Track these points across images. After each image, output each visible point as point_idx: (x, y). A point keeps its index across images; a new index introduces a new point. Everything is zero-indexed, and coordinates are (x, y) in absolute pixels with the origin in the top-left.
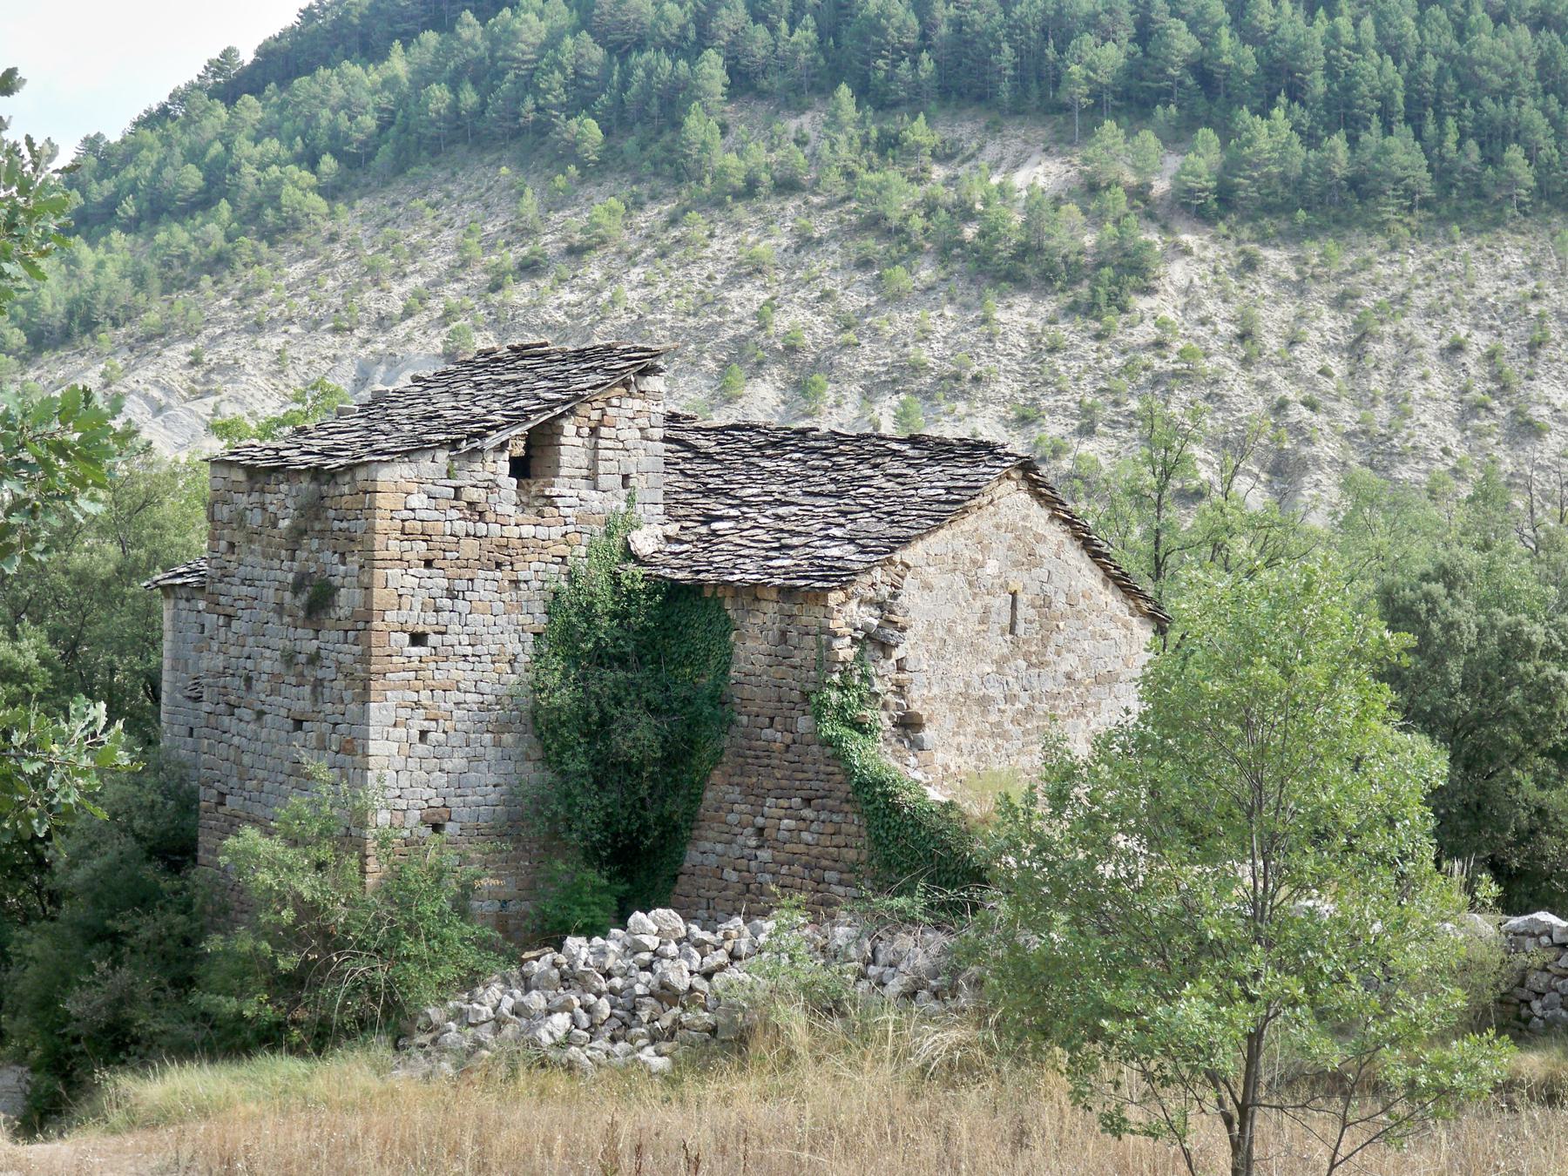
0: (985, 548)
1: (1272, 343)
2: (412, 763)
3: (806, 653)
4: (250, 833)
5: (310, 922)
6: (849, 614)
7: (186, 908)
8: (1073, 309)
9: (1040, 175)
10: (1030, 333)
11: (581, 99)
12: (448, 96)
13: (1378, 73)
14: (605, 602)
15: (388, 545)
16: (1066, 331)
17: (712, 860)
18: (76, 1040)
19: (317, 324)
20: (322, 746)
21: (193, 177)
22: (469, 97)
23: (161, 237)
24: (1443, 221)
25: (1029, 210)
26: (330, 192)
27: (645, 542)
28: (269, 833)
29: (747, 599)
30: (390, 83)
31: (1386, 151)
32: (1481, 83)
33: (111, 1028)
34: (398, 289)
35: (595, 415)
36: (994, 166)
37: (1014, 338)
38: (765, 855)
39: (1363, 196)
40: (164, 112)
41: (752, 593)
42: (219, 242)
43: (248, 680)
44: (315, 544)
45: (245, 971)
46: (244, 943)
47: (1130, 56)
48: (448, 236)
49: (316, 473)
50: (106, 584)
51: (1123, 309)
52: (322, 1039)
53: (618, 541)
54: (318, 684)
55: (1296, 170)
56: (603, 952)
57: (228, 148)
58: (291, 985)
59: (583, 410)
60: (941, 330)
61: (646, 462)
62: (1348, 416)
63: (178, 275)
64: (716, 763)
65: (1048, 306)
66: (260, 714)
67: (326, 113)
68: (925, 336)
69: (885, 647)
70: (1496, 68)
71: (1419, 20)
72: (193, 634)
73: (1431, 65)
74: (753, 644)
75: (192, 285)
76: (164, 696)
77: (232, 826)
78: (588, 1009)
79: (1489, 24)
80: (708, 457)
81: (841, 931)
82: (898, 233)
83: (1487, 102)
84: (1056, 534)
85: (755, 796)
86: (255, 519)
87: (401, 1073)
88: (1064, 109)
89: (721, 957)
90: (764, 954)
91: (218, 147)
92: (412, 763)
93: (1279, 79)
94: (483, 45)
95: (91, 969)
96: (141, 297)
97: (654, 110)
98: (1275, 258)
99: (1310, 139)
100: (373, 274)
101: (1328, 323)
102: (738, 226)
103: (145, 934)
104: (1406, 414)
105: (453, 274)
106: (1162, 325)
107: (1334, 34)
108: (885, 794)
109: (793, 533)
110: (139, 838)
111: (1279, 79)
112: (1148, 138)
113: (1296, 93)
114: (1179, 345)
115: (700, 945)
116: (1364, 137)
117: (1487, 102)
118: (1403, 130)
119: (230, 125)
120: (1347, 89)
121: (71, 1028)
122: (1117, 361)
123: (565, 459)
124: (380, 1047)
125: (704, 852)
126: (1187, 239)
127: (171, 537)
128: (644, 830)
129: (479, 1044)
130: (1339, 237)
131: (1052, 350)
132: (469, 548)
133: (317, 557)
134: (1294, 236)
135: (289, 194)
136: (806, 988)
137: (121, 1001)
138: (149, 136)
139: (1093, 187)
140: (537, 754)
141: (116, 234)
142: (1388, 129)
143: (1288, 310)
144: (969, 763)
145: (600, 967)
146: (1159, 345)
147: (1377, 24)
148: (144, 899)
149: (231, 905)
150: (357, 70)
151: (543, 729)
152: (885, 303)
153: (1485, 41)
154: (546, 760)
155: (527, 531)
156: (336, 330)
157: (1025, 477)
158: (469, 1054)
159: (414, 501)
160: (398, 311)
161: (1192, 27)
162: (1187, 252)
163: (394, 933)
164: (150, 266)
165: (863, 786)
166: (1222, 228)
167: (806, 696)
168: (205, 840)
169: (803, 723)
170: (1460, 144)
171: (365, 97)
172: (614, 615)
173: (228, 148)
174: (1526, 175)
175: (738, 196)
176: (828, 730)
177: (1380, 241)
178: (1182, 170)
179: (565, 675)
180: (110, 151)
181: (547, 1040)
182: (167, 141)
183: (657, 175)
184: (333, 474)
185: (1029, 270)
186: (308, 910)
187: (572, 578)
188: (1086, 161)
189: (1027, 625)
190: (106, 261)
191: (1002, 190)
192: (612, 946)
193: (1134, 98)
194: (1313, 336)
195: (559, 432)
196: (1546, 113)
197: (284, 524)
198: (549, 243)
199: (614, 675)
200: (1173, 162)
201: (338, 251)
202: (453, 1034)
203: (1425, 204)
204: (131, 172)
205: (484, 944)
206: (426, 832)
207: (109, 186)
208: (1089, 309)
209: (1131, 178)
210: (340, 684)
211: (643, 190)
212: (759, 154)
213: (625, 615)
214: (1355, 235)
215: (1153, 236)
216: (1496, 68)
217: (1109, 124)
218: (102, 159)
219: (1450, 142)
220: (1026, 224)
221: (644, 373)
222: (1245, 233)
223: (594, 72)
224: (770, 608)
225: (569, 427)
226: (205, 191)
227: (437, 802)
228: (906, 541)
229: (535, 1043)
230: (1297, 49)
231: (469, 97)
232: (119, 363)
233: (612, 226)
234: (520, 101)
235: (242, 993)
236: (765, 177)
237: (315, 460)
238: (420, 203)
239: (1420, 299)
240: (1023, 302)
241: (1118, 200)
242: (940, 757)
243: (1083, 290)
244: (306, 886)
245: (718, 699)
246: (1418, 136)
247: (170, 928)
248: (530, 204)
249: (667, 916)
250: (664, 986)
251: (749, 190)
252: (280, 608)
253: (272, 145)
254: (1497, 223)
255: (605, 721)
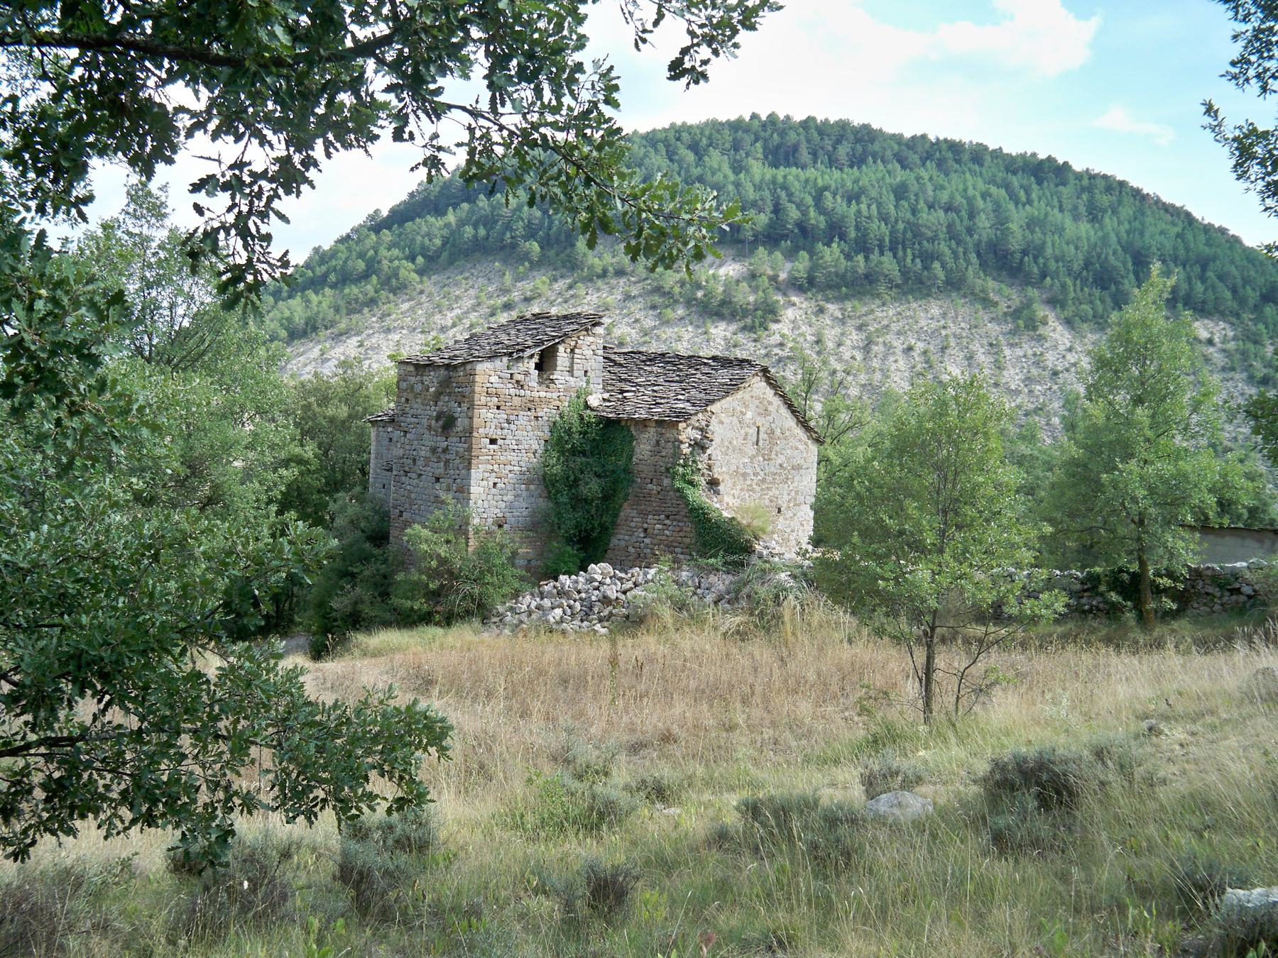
0: (747, 407)
1: (830, 345)
2: (490, 497)
3: (668, 450)
4: (417, 527)
5: (446, 570)
6: (688, 433)
7: (385, 561)
8: (744, 329)
9: (731, 270)
10: (725, 339)
11: (531, 234)
12: (473, 232)
13: (878, 229)
14: (576, 426)
15: (481, 399)
16: (741, 338)
17: (623, 543)
18: (335, 620)
19: (415, 329)
20: (448, 490)
21: (361, 265)
22: (482, 232)
23: (347, 291)
24: (905, 294)
25: (725, 285)
26: (421, 272)
27: (594, 401)
28: (425, 527)
29: (641, 427)
30: (447, 225)
31: (881, 263)
32: (922, 235)
33: (351, 615)
34: (450, 315)
35: (573, 343)
36: (711, 266)
37: (718, 340)
38: (647, 541)
39: (871, 282)
40: (348, 236)
41: (644, 423)
42: (371, 293)
43: (414, 460)
44: (447, 398)
45: (414, 589)
46: (415, 576)
47: (771, 219)
48: (472, 292)
49: (447, 366)
50: (343, 422)
51: (766, 329)
52: (448, 620)
53: (582, 400)
54: (447, 461)
55: (842, 270)
56: (576, 582)
57: (376, 252)
58: (435, 595)
59: (568, 340)
60: (686, 337)
61: (595, 366)
62: (863, 378)
63: (354, 308)
64: (626, 500)
65: (733, 327)
66: (420, 475)
67: (419, 238)
68: (679, 339)
69: (703, 448)
70: (929, 228)
71: (896, 207)
72: (386, 442)
73: (901, 226)
74: (643, 447)
75: (360, 312)
76: (573, 311)
77: (407, 524)
78: (570, 607)
79: (926, 209)
80: (621, 365)
81: (684, 573)
82: (669, 294)
83: (925, 243)
84: (777, 401)
85: (644, 514)
86: (418, 388)
87: (486, 635)
88: (742, 242)
89: (630, 584)
90: (651, 583)
91: (372, 252)
92: (490, 497)
93: (835, 230)
94: (488, 209)
95: (342, 588)
96: (338, 317)
97: (563, 238)
98: (832, 308)
99: (848, 257)
100: (439, 308)
101: (855, 337)
102: (598, 290)
103: (366, 573)
104: (888, 377)
105: (474, 309)
106: (783, 336)
107: (859, 212)
108: (704, 514)
109: (662, 398)
110: (363, 531)
111: (835, 230)
112: (778, 255)
113: (842, 237)
114: (790, 345)
115: (621, 579)
116: (872, 257)
117: (925, 243)
118: (889, 254)
119: (377, 242)
120: (864, 236)
121: (334, 614)
122: (763, 352)
123: (559, 362)
124: (476, 623)
125: (619, 539)
126: (794, 299)
127: (373, 402)
128: (593, 529)
129: (522, 622)
130: (860, 300)
131: (735, 346)
132: (517, 401)
133: (447, 404)
134: (841, 299)
135: (403, 273)
136: (670, 598)
137: (356, 603)
138: (342, 247)
139: (753, 276)
140: (545, 494)
141: (327, 290)
142: (882, 253)
143: (837, 330)
144: (737, 503)
145: (575, 588)
146: (781, 345)
147: (878, 208)
148: (366, 558)
149: (407, 559)
150: (433, 219)
151: (546, 483)
152: (662, 324)
153: (925, 217)
154: (549, 497)
155: (543, 394)
156: (422, 332)
157: (764, 375)
158: (517, 626)
159: (493, 379)
160: (450, 324)
161: (798, 207)
162: (794, 305)
163: (482, 572)
164: (342, 303)
165: (693, 510)
166: (809, 294)
167: (668, 470)
168: (394, 533)
169: (666, 482)
170: (913, 260)
171: (436, 232)
172: (581, 433)
173: (376, 252)
174: (941, 274)
175: (599, 277)
176: (678, 484)
177: (878, 302)
178: (792, 269)
179: (558, 459)
180: (324, 253)
181: (552, 620)
182: (349, 249)
183: (564, 267)
184: (455, 367)
185: (725, 311)
186: (443, 561)
187: (562, 417)
188: (751, 264)
189: (764, 442)
190: (322, 301)
191: (714, 276)
192: (581, 579)
193: (771, 238)
194: (848, 343)
195: (557, 351)
196: (950, 248)
197: (432, 390)
198: (516, 295)
199: (580, 460)
200: (788, 266)
201: (424, 298)
202: (509, 617)
203: (898, 286)
204: (334, 263)
205: (522, 579)
206: (495, 528)
207: (324, 268)
208: (751, 329)
209: (770, 272)
210: (457, 461)
211: (557, 273)
212: (608, 259)
213: (585, 433)
214: (867, 298)
215: (779, 298)
216: (929, 228)
217: (761, 248)
218: (321, 257)
219: (909, 260)
220: (724, 291)
221: (594, 325)
222: (820, 297)
223: (536, 222)
224: (652, 430)
225: (561, 348)
226: (367, 271)
227: (500, 515)
228: (713, 402)
229: (547, 621)
230: (844, 217)
231: (482, 232)
232: (328, 345)
233: (544, 289)
234: (504, 234)
235: (412, 598)
236: (611, 269)
237: (446, 362)
238: (460, 277)
239: (895, 327)
240: (722, 325)
241: (764, 281)
242: (726, 499)
243: (749, 320)
244: (443, 551)
245: (627, 471)
246: (895, 257)
247: (378, 570)
248: (508, 278)
249: (606, 566)
250: (605, 597)
251: (604, 274)
252: (430, 428)
253: (396, 252)
254: (928, 295)
255: (576, 480)
